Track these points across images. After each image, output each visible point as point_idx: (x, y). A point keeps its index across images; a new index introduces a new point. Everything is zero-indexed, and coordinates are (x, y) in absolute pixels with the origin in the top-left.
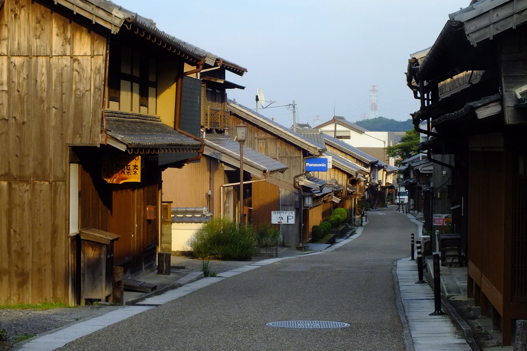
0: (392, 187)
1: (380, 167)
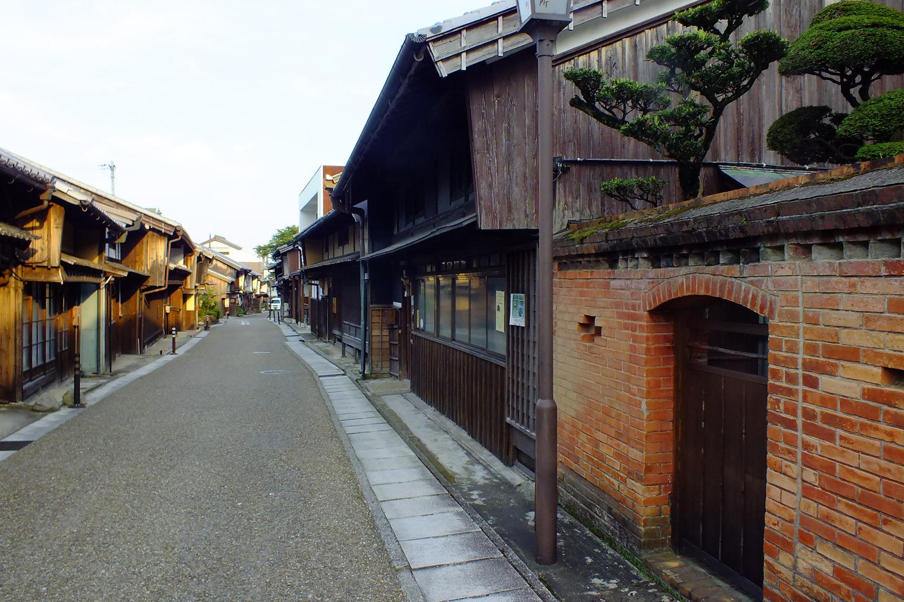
0: (266, 296)
1: (254, 277)
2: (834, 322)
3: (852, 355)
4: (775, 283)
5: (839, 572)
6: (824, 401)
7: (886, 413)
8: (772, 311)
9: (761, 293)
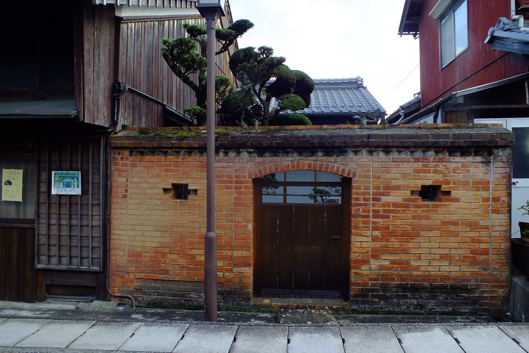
2: (389, 178)
3: (397, 188)
4: (356, 164)
5: (393, 262)
6: (384, 205)
7: (413, 205)
8: (354, 175)
9: (347, 169)
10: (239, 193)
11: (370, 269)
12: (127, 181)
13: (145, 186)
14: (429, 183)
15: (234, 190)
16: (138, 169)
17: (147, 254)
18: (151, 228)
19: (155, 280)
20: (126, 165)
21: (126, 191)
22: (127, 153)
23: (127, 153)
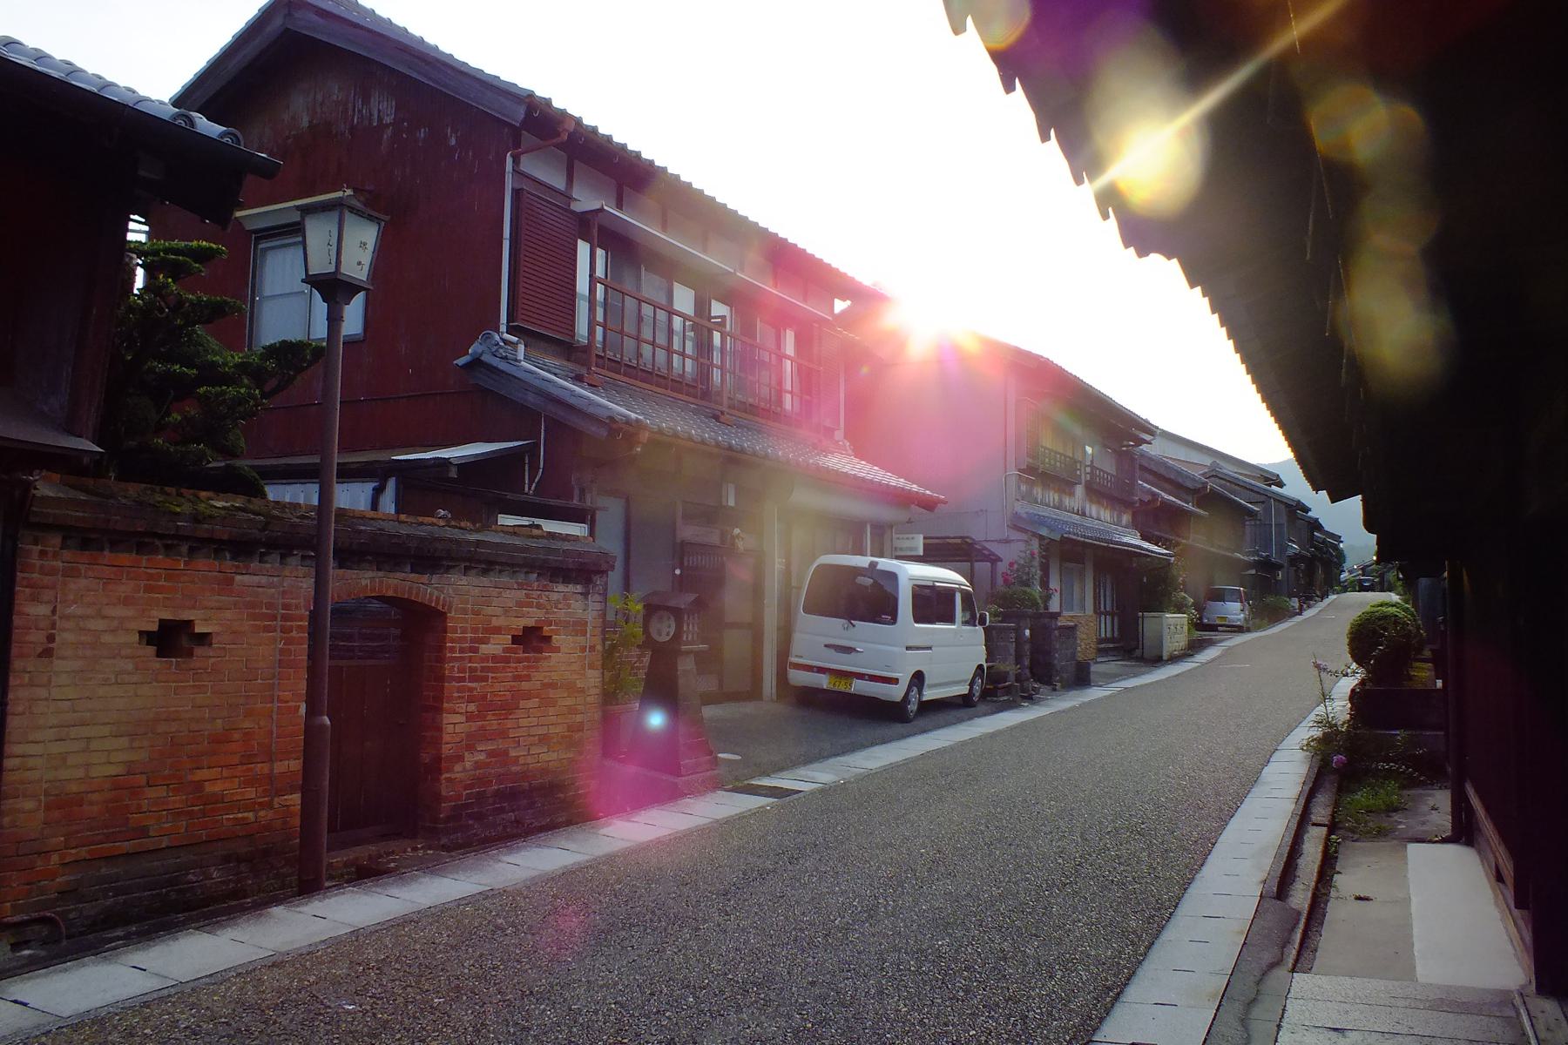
3: (498, 630)
10: (289, 642)
11: (464, 770)
12: (54, 612)
13: (99, 625)
14: (531, 622)
15: (278, 634)
16: (83, 582)
17: (95, 797)
18: (106, 730)
19: (109, 859)
20: (52, 572)
21: (51, 638)
22: (56, 540)
23: (56, 540)
